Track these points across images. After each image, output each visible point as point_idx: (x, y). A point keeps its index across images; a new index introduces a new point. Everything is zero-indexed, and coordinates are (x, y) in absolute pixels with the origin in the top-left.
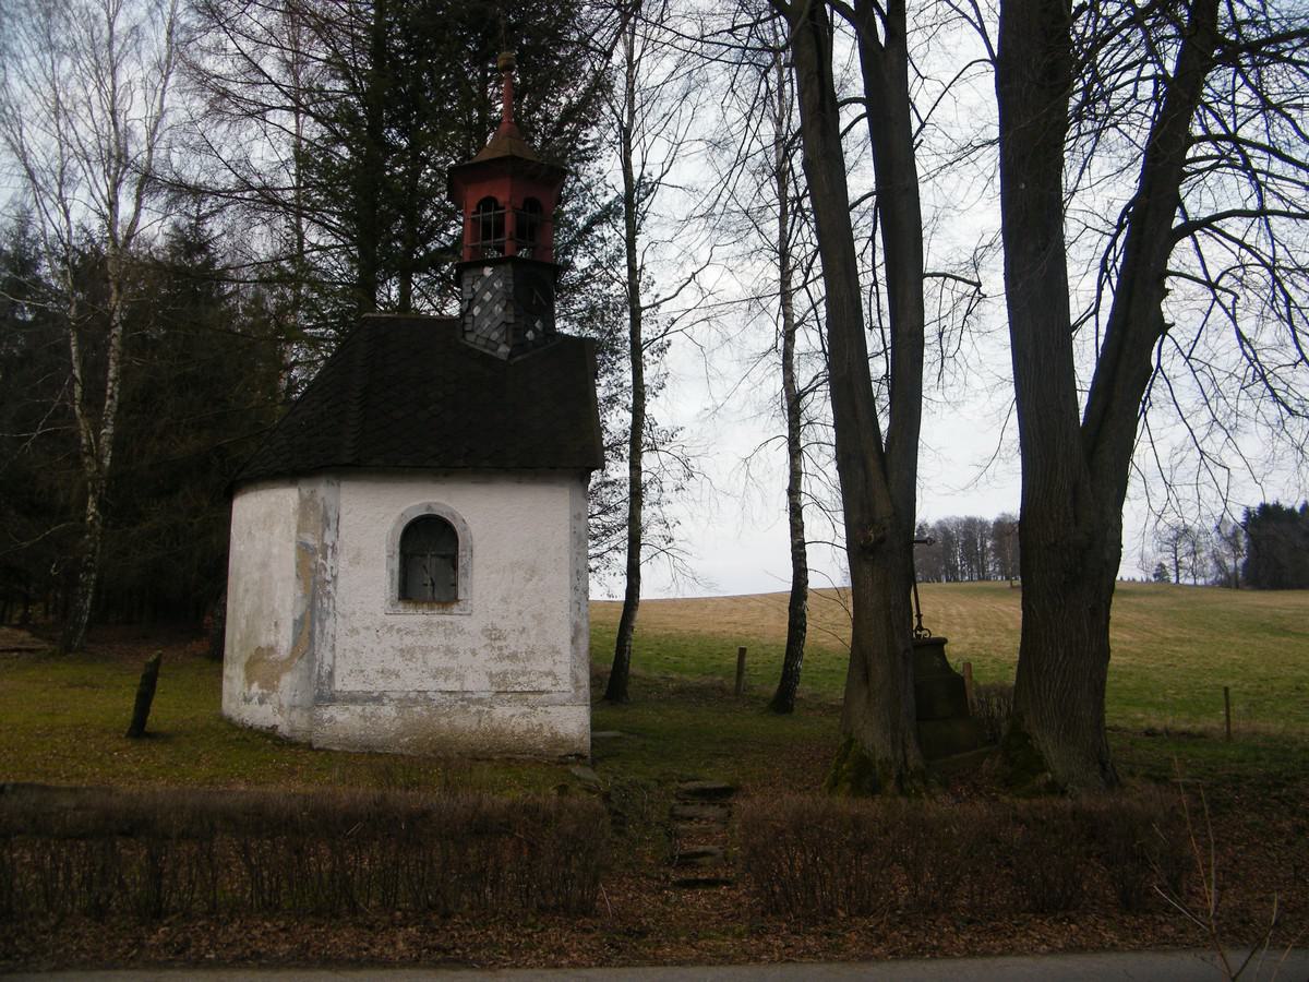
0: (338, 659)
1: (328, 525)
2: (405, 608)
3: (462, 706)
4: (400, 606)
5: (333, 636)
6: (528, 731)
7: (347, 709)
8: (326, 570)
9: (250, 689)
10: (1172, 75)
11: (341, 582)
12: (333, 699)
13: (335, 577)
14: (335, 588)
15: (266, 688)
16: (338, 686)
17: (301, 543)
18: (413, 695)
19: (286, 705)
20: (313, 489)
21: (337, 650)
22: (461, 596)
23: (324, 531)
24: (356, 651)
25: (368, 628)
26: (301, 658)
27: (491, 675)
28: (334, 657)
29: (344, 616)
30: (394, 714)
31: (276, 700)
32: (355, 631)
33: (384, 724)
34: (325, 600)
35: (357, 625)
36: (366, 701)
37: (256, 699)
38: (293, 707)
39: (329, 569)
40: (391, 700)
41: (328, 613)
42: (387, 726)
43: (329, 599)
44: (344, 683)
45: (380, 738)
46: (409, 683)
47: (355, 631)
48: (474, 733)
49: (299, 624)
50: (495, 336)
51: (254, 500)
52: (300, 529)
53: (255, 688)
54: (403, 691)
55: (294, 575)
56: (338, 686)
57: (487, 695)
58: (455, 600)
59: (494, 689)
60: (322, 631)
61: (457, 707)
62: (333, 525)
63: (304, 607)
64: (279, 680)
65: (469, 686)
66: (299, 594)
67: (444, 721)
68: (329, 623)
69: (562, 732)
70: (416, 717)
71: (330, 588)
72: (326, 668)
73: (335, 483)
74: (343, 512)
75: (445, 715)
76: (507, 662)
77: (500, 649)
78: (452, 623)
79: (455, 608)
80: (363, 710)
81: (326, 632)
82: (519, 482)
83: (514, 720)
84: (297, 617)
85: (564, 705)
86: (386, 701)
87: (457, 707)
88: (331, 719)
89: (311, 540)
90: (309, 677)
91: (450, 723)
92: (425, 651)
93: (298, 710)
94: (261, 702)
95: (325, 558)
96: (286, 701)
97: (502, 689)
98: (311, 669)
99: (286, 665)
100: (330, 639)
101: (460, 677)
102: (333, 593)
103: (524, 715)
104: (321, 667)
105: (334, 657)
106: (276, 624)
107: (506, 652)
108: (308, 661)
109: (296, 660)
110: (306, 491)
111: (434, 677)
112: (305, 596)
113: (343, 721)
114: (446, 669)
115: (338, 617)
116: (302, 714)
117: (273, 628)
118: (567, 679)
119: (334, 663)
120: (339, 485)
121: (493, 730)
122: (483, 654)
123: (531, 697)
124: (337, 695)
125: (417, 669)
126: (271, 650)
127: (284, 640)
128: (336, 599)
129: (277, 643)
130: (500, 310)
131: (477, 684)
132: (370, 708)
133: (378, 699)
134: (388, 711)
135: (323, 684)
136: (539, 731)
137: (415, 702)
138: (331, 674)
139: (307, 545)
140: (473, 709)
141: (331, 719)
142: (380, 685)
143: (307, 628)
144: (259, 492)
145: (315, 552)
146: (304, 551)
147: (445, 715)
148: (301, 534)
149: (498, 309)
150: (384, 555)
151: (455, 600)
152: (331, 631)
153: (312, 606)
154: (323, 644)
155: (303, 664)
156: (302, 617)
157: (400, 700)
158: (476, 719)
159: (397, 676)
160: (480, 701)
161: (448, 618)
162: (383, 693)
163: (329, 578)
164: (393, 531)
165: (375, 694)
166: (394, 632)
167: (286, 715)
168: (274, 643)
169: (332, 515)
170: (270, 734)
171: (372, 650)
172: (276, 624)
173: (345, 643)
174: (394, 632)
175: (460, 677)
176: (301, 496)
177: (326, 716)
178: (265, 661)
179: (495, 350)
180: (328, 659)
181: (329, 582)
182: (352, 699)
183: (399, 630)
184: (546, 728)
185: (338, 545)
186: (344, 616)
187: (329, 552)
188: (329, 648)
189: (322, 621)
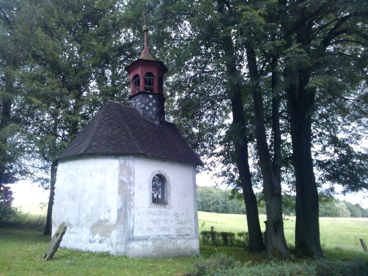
0: (135, 224)
1: (131, 174)
2: (154, 205)
3: (169, 240)
4: (153, 204)
5: (134, 216)
6: (186, 248)
7: (138, 243)
8: (131, 191)
9: (93, 237)
10: (306, 88)
11: (135, 195)
12: (133, 240)
13: (134, 194)
14: (134, 198)
15: (104, 236)
16: (135, 234)
17: (121, 180)
18: (156, 237)
19: (114, 243)
20: (125, 161)
21: (135, 221)
22: (169, 202)
23: (130, 176)
24: (140, 221)
25: (143, 213)
26: (121, 224)
27: (176, 229)
28: (134, 223)
29: (136, 208)
30: (151, 244)
31: (109, 241)
32: (140, 214)
33: (149, 248)
34: (131, 202)
35: (141, 211)
36: (143, 240)
37: (98, 241)
38: (117, 244)
39: (132, 190)
40: (150, 239)
41: (132, 207)
42: (150, 249)
43: (132, 201)
44: (137, 233)
45: (147, 254)
46: (155, 233)
47: (140, 214)
48: (172, 250)
49: (119, 211)
50: (154, 117)
51: (95, 162)
52: (120, 175)
53: (97, 236)
54: (154, 236)
55: (117, 192)
56: (135, 234)
57: (175, 236)
58: (167, 204)
59: (177, 234)
60: (130, 214)
61: (168, 241)
62: (133, 175)
63: (122, 204)
64: (110, 232)
65: (171, 233)
66: (120, 199)
67: (165, 246)
68: (132, 210)
69: (193, 249)
70: (158, 245)
71: (132, 197)
72: (131, 228)
73: (133, 159)
74: (136, 170)
75: (165, 244)
76: (180, 225)
77: (178, 220)
78: (166, 211)
79: (167, 206)
80: (143, 243)
81: (131, 214)
82: (181, 166)
83: (182, 245)
84: (119, 208)
85: (193, 239)
86: (149, 239)
87: (168, 241)
88: (133, 248)
89: (125, 180)
90: (124, 232)
91: (166, 247)
92: (159, 221)
93: (120, 245)
94: (100, 242)
95: (131, 186)
96: (114, 241)
97: (179, 234)
98: (125, 228)
99: (114, 227)
100: (132, 216)
101: (169, 230)
102: (133, 200)
103: (184, 243)
104: (129, 227)
105: (134, 223)
106: (109, 211)
107: (180, 221)
108: (124, 225)
109: (119, 225)
110: (122, 161)
111: (162, 230)
112: (122, 200)
113: (137, 248)
114: (165, 227)
115: (135, 208)
116: (121, 246)
117: (107, 212)
118: (194, 230)
119: (134, 226)
120: (134, 161)
121: (178, 249)
122: (174, 222)
123: (186, 236)
124: (135, 238)
125: (157, 228)
126: (107, 221)
127: (113, 217)
128: (134, 202)
129: (109, 218)
130: (155, 109)
131: (173, 233)
132: (145, 242)
133: (147, 239)
134: (150, 243)
135: (130, 234)
136: (188, 248)
137: (157, 239)
138: (133, 230)
139: (123, 181)
140: (172, 241)
141: (133, 248)
142: (147, 234)
143: (123, 212)
144: (97, 160)
145: (126, 184)
146: (121, 183)
147: (165, 244)
148: (121, 177)
149: (154, 109)
150: (148, 187)
151: (167, 204)
152: (133, 214)
153: (125, 204)
154: (130, 219)
155: (122, 227)
156: (121, 208)
157: (153, 239)
158: (173, 245)
159: (152, 230)
160: (173, 238)
161: (165, 209)
162: (148, 237)
163: (132, 194)
164: (169, 180)
165: (146, 237)
166: (151, 214)
167: (114, 247)
168: (108, 219)
169: (132, 171)
170: (106, 255)
171: (145, 221)
172: (109, 211)
173: (137, 218)
174: (151, 214)
175: (169, 230)
176: (120, 163)
177: (131, 247)
178: (103, 225)
179: (154, 122)
180: (132, 225)
181: (132, 195)
182: (139, 239)
183: (152, 214)
184: (190, 247)
185: (134, 182)
186: (136, 208)
187: (132, 184)
188: (132, 220)
189: (130, 210)
